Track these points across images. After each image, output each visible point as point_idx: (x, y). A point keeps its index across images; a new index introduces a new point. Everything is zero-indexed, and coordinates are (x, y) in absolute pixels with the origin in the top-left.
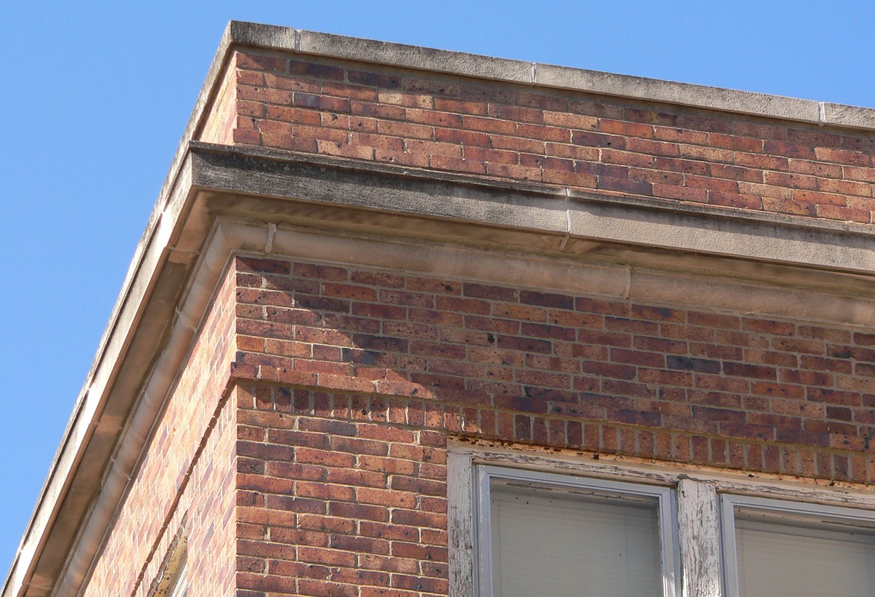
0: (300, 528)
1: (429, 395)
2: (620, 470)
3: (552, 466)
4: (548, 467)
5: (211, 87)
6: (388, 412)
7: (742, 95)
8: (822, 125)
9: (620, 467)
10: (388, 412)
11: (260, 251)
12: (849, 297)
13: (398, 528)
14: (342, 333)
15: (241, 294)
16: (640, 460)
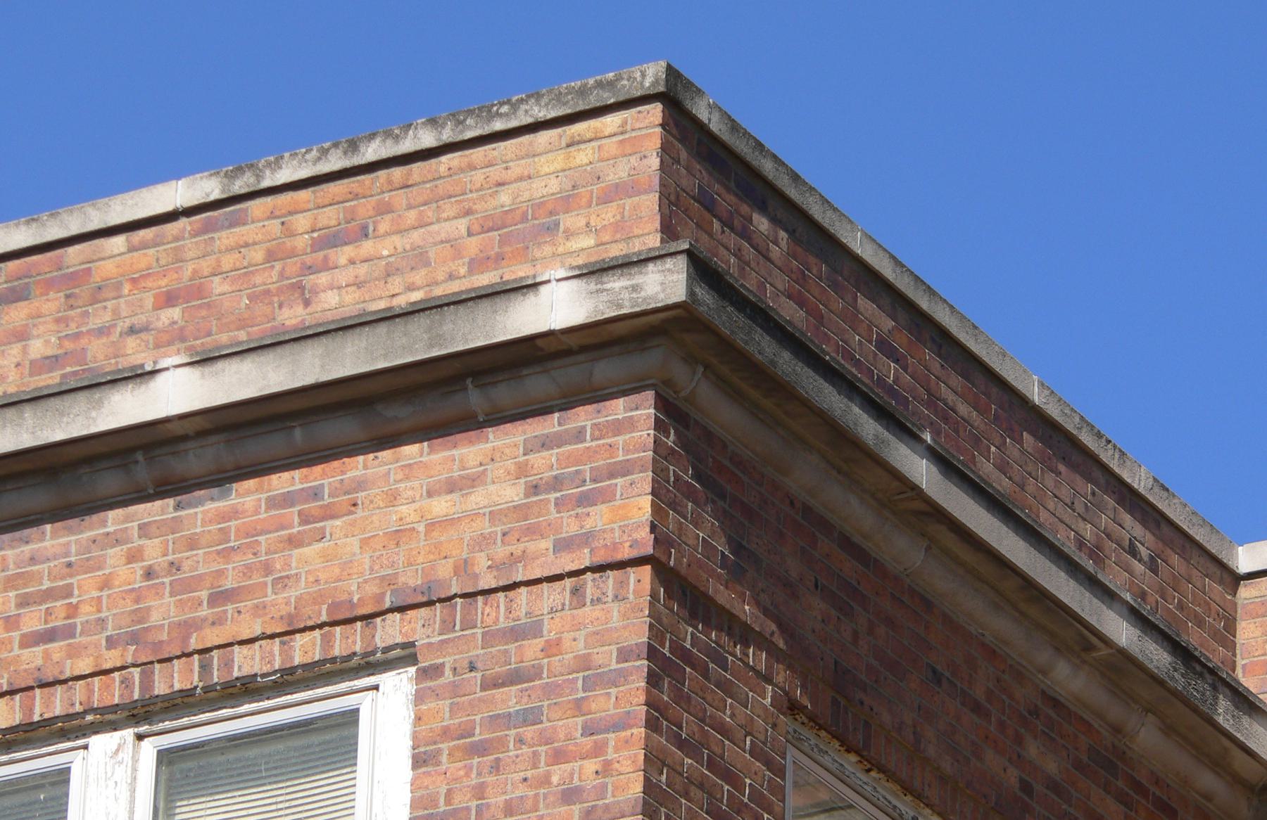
0: (687, 778)
1: (781, 644)
2: (877, 792)
3: (833, 767)
4: (831, 765)
5: (569, 111)
6: (751, 650)
7: (989, 342)
8: (1030, 405)
9: (879, 789)
10: (751, 650)
11: (675, 392)
12: (1061, 648)
13: (752, 808)
14: (722, 529)
15: (277, 310)
16: (896, 788)
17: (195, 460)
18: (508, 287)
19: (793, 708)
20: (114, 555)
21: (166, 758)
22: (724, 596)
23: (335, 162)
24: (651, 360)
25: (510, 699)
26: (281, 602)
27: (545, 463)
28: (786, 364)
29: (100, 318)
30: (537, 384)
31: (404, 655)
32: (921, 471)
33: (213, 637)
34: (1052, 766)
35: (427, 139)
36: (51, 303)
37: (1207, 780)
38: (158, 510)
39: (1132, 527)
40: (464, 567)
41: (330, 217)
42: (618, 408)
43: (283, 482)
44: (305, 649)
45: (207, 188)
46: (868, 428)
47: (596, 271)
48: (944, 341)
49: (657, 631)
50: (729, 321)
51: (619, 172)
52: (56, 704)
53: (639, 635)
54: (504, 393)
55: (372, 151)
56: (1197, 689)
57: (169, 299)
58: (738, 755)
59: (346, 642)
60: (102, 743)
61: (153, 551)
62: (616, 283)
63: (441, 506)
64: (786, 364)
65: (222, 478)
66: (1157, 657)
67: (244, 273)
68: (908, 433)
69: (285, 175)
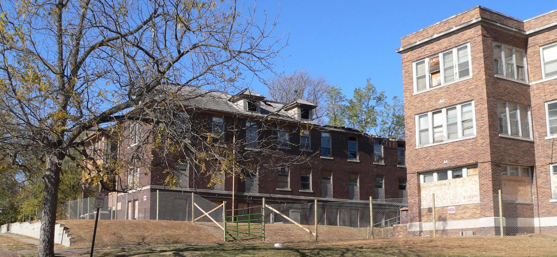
17: (457, 32)
18: (454, 104)
22: (487, 35)
24: (480, 23)
25: (475, 44)
30: (474, 25)
31: (469, 42)
32: (499, 25)
34: (511, 38)
37: (522, 36)
38: (455, 35)
39: (516, 22)
42: (479, 26)
43: (462, 33)
44: (464, 42)
45: (455, 16)
46: (495, 23)
47: (476, 19)
49: (482, 39)
51: (477, 12)
52: (451, 47)
54: (472, 26)
55: (464, 13)
56: (520, 31)
59: (466, 42)
60: (454, 49)
61: (455, 38)
62: (477, 19)
63: (470, 33)
65: (458, 33)
66: (517, 30)
68: (497, 23)
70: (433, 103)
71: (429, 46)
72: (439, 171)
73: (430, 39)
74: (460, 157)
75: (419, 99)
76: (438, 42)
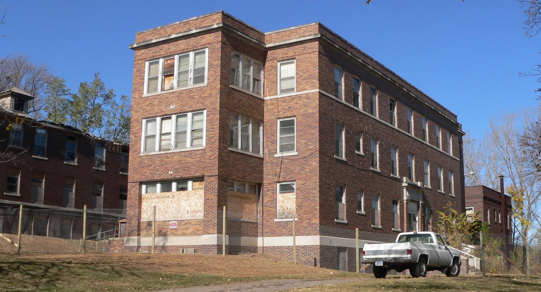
19: (232, 49)
20: (191, 41)
21: (195, 53)
22: (227, 43)
23: (204, 16)
25: (213, 50)
26: (201, 44)
27: (215, 35)
28: (230, 28)
29: (190, 26)
30: (215, 31)
31: (208, 47)
32: (240, 33)
33: (197, 46)
35: (209, 15)
36: (188, 25)
37: (262, 48)
38: (194, 38)
39: (257, 33)
40: (211, 42)
41: (203, 20)
42: (219, 32)
44: (202, 47)
45: (196, 18)
46: (236, 31)
47: (217, 24)
48: (243, 24)
49: (222, 46)
50: (226, 27)
51: (219, 17)
53: (220, 46)
54: (213, 31)
55: (206, 16)
56: (260, 44)
57: (194, 25)
58: (228, 53)
59: (204, 46)
60: (191, 52)
61: (194, 41)
62: (219, 25)
63: (210, 38)
64: (230, 28)
65: (197, 36)
66: (257, 42)
67: (198, 23)
68: (238, 31)
69: (201, 17)
70: (163, 108)
71: (165, 46)
72: (162, 182)
73: (167, 38)
74: (186, 169)
75: (148, 102)
76: (175, 43)
